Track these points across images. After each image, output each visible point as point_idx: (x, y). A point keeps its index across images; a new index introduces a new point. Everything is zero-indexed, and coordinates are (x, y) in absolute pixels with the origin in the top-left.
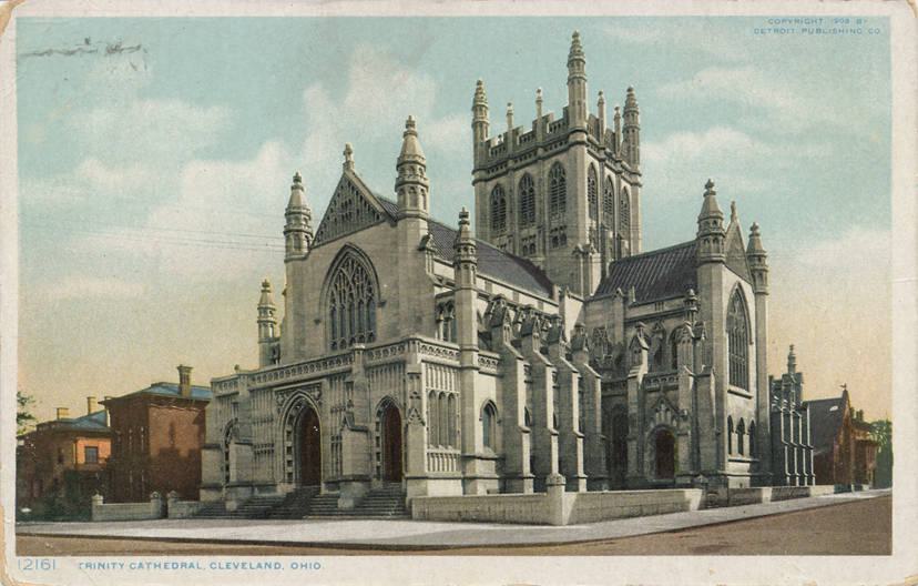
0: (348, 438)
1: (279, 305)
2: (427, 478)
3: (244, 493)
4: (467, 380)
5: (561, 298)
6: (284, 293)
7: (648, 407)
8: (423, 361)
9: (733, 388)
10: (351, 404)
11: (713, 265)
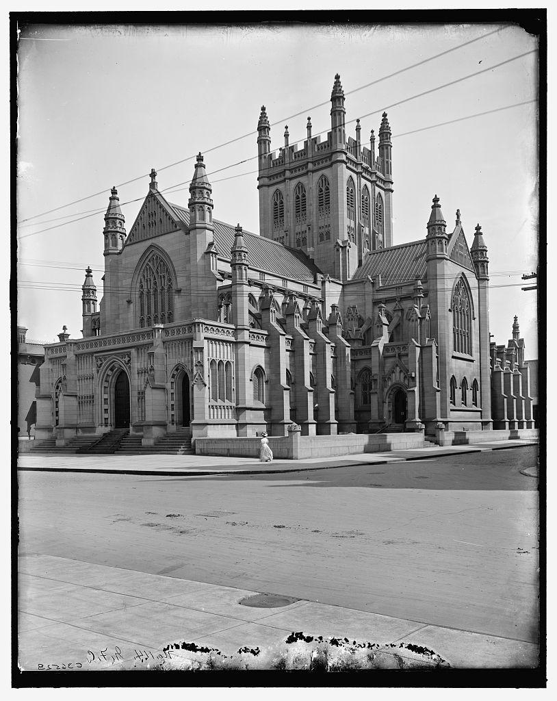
0: (150, 395)
1: (97, 282)
2: (208, 424)
3: (69, 433)
4: (240, 351)
5: (323, 283)
6: (103, 279)
7: (387, 370)
8: (205, 338)
9: (457, 354)
10: (152, 369)
11: (437, 260)
